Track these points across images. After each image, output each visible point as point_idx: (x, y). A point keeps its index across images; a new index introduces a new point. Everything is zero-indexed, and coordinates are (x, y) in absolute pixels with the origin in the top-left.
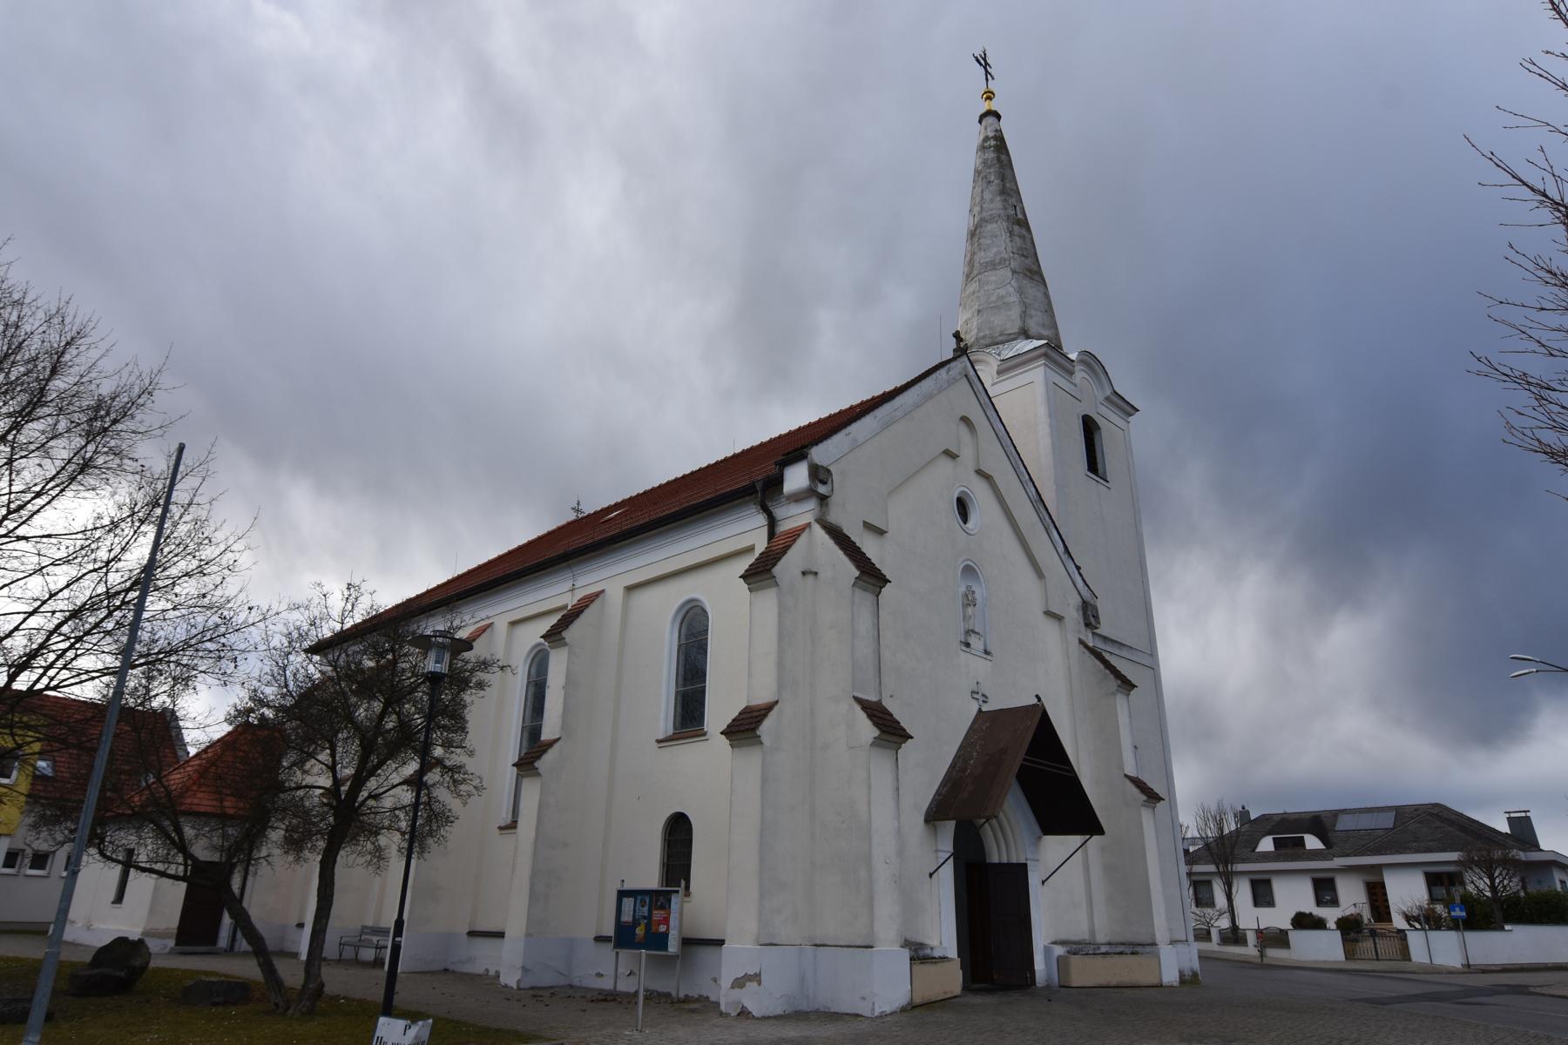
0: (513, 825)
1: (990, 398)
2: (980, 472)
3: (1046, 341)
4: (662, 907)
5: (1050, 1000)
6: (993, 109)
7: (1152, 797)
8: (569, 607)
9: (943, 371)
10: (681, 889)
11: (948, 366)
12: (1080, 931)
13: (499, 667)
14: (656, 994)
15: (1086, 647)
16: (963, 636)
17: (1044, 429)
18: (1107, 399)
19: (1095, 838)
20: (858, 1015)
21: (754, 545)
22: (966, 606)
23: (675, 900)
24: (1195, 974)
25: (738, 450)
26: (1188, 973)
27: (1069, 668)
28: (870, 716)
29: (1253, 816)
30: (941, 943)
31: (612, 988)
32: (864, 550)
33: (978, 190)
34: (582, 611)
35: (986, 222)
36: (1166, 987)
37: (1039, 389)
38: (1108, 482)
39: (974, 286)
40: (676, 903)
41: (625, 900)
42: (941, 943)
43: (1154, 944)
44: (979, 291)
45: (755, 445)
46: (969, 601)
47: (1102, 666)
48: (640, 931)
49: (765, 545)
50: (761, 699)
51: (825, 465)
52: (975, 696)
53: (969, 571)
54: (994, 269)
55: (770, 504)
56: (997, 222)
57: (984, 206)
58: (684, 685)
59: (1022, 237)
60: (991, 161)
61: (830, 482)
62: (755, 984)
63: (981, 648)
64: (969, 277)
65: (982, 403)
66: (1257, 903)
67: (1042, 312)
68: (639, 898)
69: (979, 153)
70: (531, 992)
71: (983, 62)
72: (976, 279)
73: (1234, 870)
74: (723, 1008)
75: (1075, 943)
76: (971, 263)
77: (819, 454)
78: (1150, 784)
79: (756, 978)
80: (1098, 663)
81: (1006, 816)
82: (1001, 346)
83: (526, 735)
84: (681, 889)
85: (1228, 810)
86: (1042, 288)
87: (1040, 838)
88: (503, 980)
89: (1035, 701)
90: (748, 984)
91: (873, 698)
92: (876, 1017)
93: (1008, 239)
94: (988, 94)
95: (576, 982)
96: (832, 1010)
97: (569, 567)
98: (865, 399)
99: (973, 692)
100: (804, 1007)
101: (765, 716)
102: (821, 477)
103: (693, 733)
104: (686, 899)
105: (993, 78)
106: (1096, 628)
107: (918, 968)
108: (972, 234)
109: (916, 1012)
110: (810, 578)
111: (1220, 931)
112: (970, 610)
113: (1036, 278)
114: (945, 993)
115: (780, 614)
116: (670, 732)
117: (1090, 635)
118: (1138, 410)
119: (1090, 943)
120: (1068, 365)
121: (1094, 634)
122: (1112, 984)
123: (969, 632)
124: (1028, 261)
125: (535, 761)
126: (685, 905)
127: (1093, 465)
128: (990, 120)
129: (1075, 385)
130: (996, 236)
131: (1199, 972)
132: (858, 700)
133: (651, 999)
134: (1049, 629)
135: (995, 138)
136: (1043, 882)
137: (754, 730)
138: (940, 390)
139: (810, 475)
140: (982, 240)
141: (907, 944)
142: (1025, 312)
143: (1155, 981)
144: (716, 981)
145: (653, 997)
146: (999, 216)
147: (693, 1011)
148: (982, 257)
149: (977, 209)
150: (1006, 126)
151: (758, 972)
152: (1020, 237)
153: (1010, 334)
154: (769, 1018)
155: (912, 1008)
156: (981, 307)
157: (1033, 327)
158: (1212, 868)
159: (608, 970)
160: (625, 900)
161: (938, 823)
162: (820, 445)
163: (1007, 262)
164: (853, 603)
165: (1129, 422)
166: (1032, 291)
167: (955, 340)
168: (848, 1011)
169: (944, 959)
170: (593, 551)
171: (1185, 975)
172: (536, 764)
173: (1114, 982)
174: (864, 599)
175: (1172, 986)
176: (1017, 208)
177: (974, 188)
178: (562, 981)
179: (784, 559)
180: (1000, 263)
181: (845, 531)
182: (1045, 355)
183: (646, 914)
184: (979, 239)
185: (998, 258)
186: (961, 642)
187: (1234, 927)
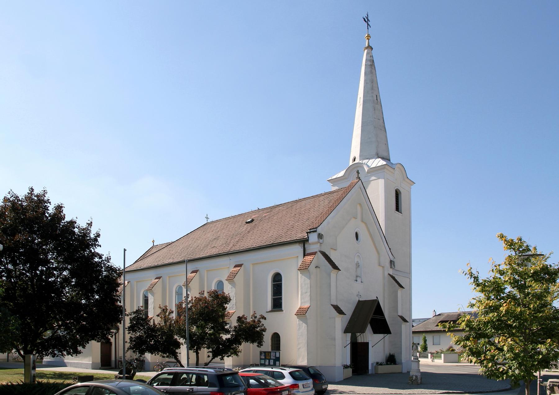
89: (376, 298)
110: (318, 269)
123: (357, 277)
127: (398, 209)
132: (332, 305)
136: (372, 347)
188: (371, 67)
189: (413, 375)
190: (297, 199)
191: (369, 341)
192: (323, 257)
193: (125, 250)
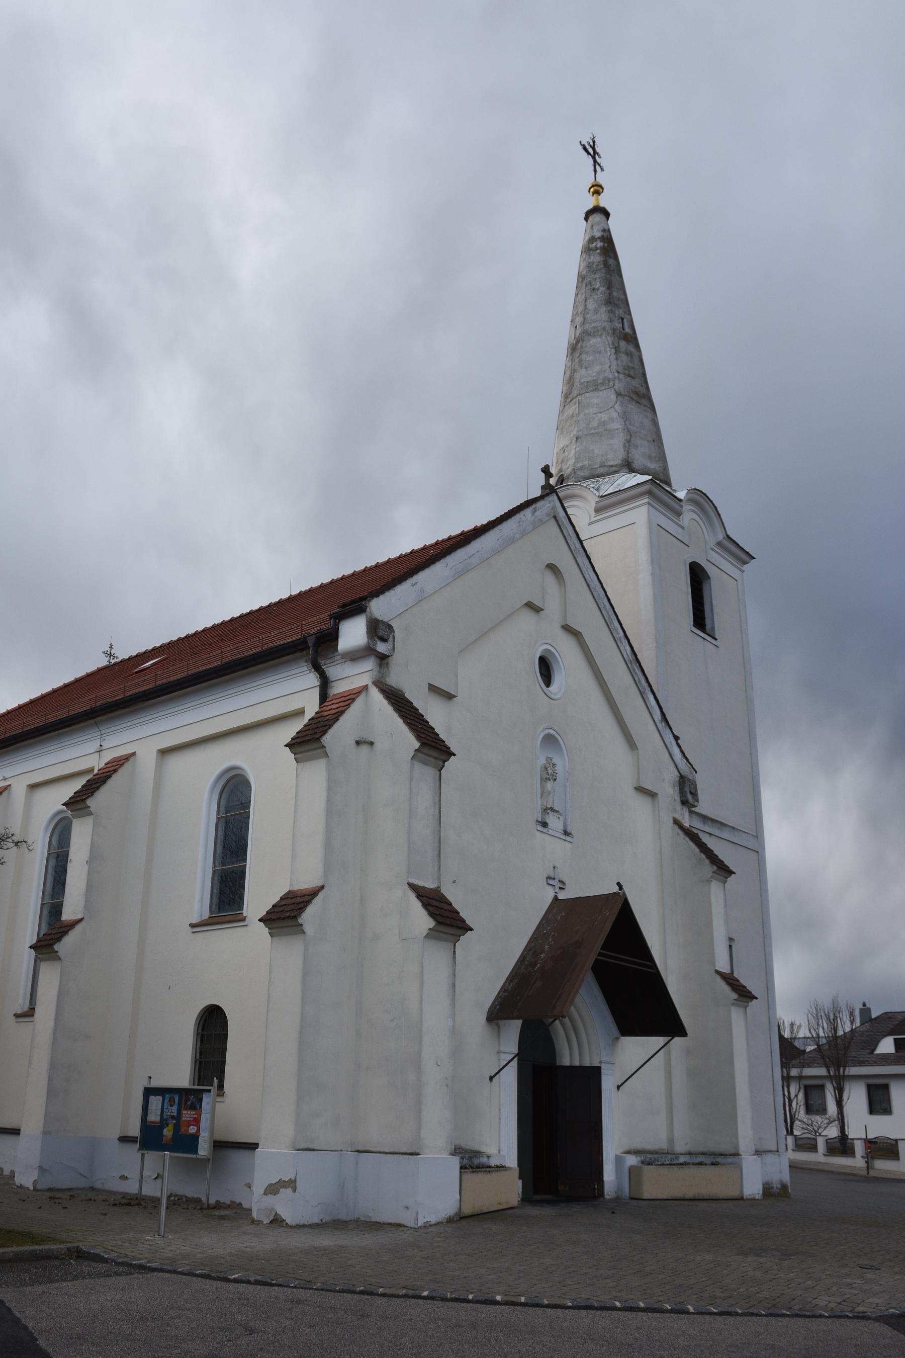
0: (30, 1013)
1: (581, 542)
2: (567, 628)
3: (650, 477)
4: (193, 1107)
5: (613, 1213)
6: (602, 205)
7: (744, 995)
8: (96, 771)
9: (528, 512)
10: (214, 1089)
11: (534, 506)
12: (656, 1139)
13: (13, 842)
14: (184, 1200)
15: (681, 827)
16: (540, 815)
17: (645, 577)
18: (719, 544)
19: (677, 1040)
20: (399, 1225)
21: (304, 708)
22: (544, 780)
23: (206, 1100)
24: (784, 1187)
25: (295, 592)
26: (776, 1185)
27: (661, 852)
28: (425, 906)
29: (874, 1015)
30: (499, 1151)
31: (137, 1192)
32: (428, 717)
33: (581, 298)
34: (110, 777)
35: (590, 335)
36: (748, 1200)
37: (641, 531)
38: (716, 639)
39: (573, 409)
40: (208, 1103)
41: (152, 1099)
42: (499, 1151)
43: (737, 1154)
44: (578, 415)
45: (314, 586)
46: (549, 775)
47: (697, 850)
48: (168, 1132)
49: (317, 709)
50: (305, 883)
51: (386, 619)
52: (551, 882)
53: (550, 740)
54: (596, 390)
55: (323, 662)
56: (601, 335)
57: (587, 316)
58: (223, 864)
59: (629, 354)
60: (598, 266)
61: (391, 639)
62: (289, 1190)
63: (560, 827)
64: (567, 397)
65: (573, 548)
66: (872, 1111)
67: (648, 441)
68: (167, 1096)
69: (584, 255)
70: (49, 1194)
71: (591, 150)
72: (576, 400)
73: (846, 1073)
74: (255, 1215)
75: (650, 1152)
76: (570, 381)
77: (379, 607)
78: (743, 982)
79: (291, 1184)
80: (693, 846)
81: (577, 1011)
82: (600, 479)
83: (45, 912)
84: (214, 1089)
85: (844, 1008)
86: (649, 414)
87: (617, 1038)
88: (19, 1180)
89: (616, 889)
90: (282, 1190)
91: (430, 884)
92: (420, 1227)
93: (613, 357)
94: (596, 188)
95: (98, 1185)
96: (373, 1220)
97: (96, 724)
98: (440, 539)
99: (549, 878)
100: (343, 1216)
101: (308, 902)
102: (381, 633)
103: (228, 918)
104: (219, 1099)
105: (602, 170)
106: (695, 806)
107: (468, 1176)
108: (574, 348)
109: (464, 1223)
110: (365, 749)
111: (827, 1140)
112: (549, 785)
113: (644, 401)
114: (500, 1204)
115: (329, 789)
116: (206, 915)
117: (687, 814)
118: (754, 558)
119: (668, 1153)
120: (677, 507)
121: (691, 812)
122: (687, 1197)
123: (548, 810)
124: (635, 383)
125: (55, 943)
126: (218, 1105)
127: (700, 620)
128: (597, 218)
129: (683, 528)
130: (600, 353)
131: (789, 1185)
132: (413, 887)
133: (179, 1205)
134: (640, 807)
135: (602, 239)
136: (618, 1087)
137: (295, 918)
138: (524, 534)
139: (368, 632)
140: (584, 356)
141: (457, 1151)
142: (629, 441)
143: (735, 1193)
144: (250, 1187)
145: (177, 1202)
146: (604, 329)
147: (223, 1218)
148: (583, 375)
149: (579, 320)
150: (613, 224)
151: (293, 1178)
152: (627, 354)
153: (612, 466)
154: (304, 1226)
155: (460, 1218)
156: (580, 433)
157: (639, 460)
158: (822, 1071)
159: (133, 1173)
160: (152, 1099)
161: (501, 1022)
162: (381, 597)
163: (611, 383)
164: (411, 779)
165: (743, 572)
166: (638, 416)
167: (543, 475)
168: (390, 1221)
169: (501, 1168)
170: (124, 708)
171: (772, 1188)
172: (56, 947)
173: (690, 1195)
174: (425, 773)
175: (754, 1199)
176: (625, 320)
177: (577, 295)
178: (83, 1183)
179: (336, 726)
180: (603, 384)
181: (408, 695)
182: (649, 493)
183: (175, 1114)
184: (580, 354)
185: (601, 377)
186: (537, 821)
187: (843, 1137)
191: (601, 1062)
192: (385, 702)
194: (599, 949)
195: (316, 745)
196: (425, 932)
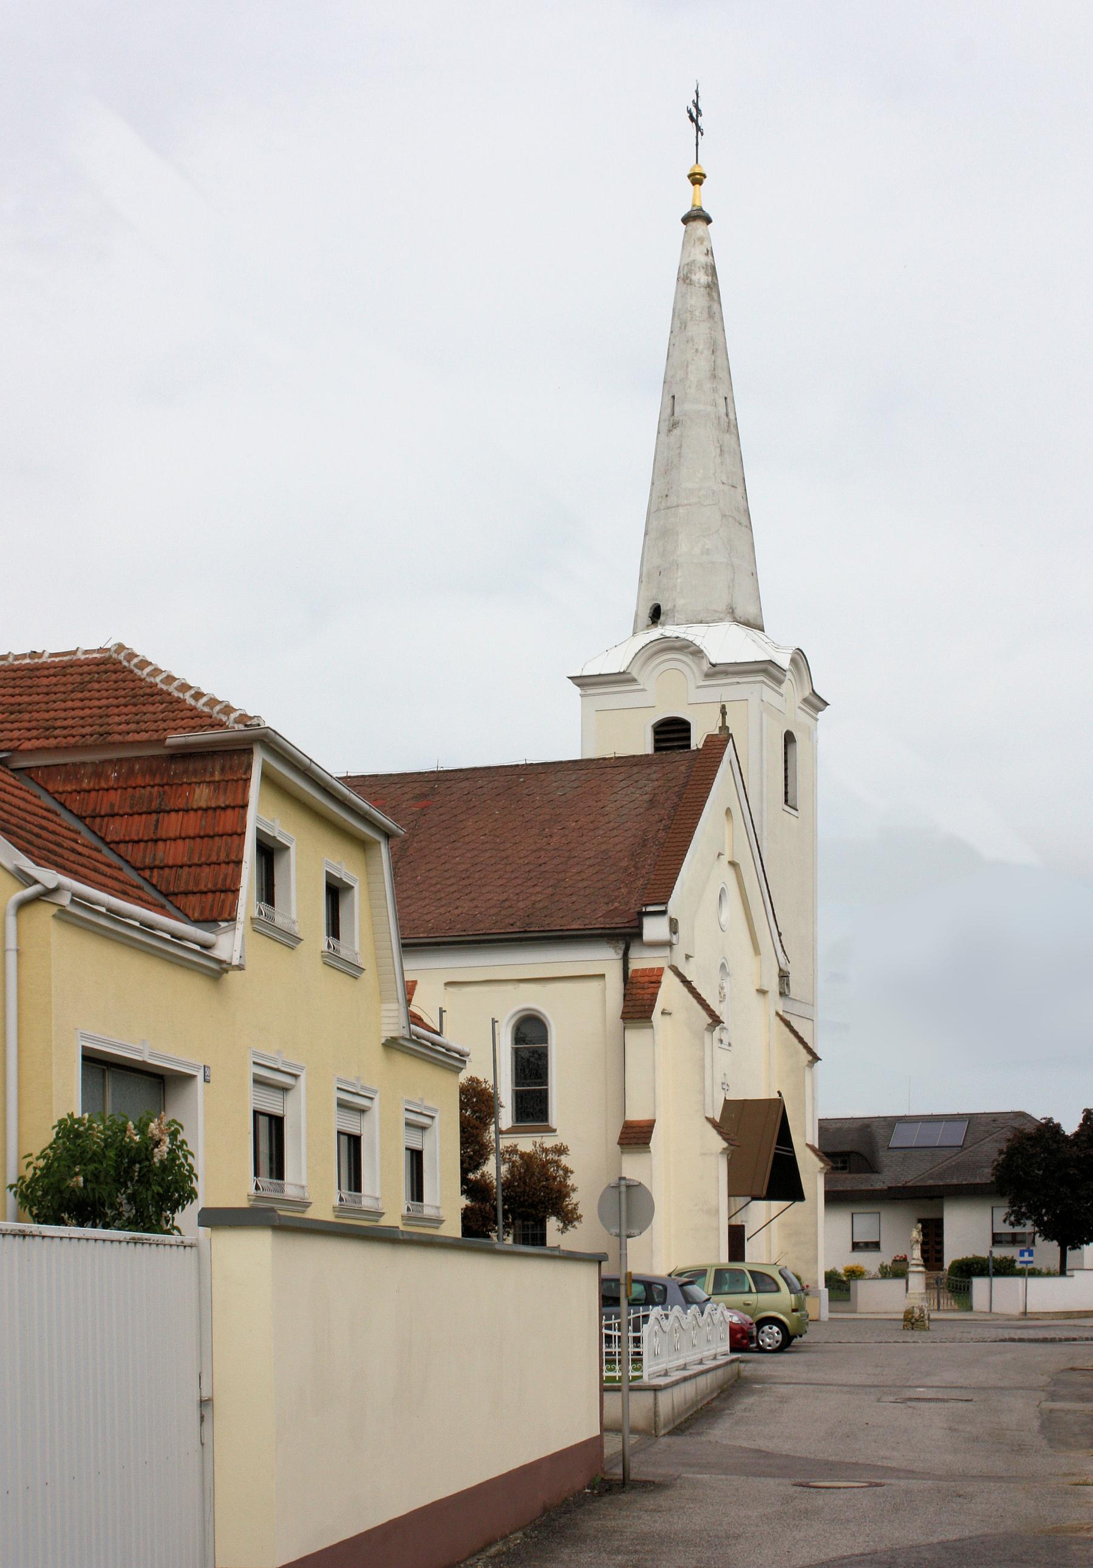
38: (797, 810)
188: (709, 294)
189: (913, 1307)
190: (520, 763)
193: (494, 1022)
194: (774, 1145)
195: (648, 1020)
196: (720, 1150)
